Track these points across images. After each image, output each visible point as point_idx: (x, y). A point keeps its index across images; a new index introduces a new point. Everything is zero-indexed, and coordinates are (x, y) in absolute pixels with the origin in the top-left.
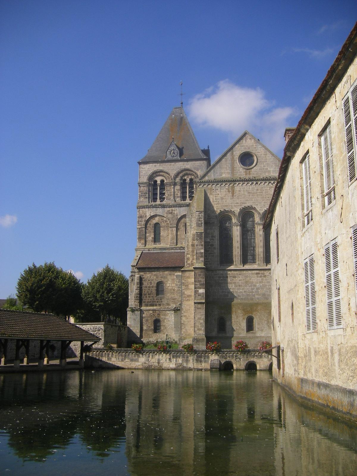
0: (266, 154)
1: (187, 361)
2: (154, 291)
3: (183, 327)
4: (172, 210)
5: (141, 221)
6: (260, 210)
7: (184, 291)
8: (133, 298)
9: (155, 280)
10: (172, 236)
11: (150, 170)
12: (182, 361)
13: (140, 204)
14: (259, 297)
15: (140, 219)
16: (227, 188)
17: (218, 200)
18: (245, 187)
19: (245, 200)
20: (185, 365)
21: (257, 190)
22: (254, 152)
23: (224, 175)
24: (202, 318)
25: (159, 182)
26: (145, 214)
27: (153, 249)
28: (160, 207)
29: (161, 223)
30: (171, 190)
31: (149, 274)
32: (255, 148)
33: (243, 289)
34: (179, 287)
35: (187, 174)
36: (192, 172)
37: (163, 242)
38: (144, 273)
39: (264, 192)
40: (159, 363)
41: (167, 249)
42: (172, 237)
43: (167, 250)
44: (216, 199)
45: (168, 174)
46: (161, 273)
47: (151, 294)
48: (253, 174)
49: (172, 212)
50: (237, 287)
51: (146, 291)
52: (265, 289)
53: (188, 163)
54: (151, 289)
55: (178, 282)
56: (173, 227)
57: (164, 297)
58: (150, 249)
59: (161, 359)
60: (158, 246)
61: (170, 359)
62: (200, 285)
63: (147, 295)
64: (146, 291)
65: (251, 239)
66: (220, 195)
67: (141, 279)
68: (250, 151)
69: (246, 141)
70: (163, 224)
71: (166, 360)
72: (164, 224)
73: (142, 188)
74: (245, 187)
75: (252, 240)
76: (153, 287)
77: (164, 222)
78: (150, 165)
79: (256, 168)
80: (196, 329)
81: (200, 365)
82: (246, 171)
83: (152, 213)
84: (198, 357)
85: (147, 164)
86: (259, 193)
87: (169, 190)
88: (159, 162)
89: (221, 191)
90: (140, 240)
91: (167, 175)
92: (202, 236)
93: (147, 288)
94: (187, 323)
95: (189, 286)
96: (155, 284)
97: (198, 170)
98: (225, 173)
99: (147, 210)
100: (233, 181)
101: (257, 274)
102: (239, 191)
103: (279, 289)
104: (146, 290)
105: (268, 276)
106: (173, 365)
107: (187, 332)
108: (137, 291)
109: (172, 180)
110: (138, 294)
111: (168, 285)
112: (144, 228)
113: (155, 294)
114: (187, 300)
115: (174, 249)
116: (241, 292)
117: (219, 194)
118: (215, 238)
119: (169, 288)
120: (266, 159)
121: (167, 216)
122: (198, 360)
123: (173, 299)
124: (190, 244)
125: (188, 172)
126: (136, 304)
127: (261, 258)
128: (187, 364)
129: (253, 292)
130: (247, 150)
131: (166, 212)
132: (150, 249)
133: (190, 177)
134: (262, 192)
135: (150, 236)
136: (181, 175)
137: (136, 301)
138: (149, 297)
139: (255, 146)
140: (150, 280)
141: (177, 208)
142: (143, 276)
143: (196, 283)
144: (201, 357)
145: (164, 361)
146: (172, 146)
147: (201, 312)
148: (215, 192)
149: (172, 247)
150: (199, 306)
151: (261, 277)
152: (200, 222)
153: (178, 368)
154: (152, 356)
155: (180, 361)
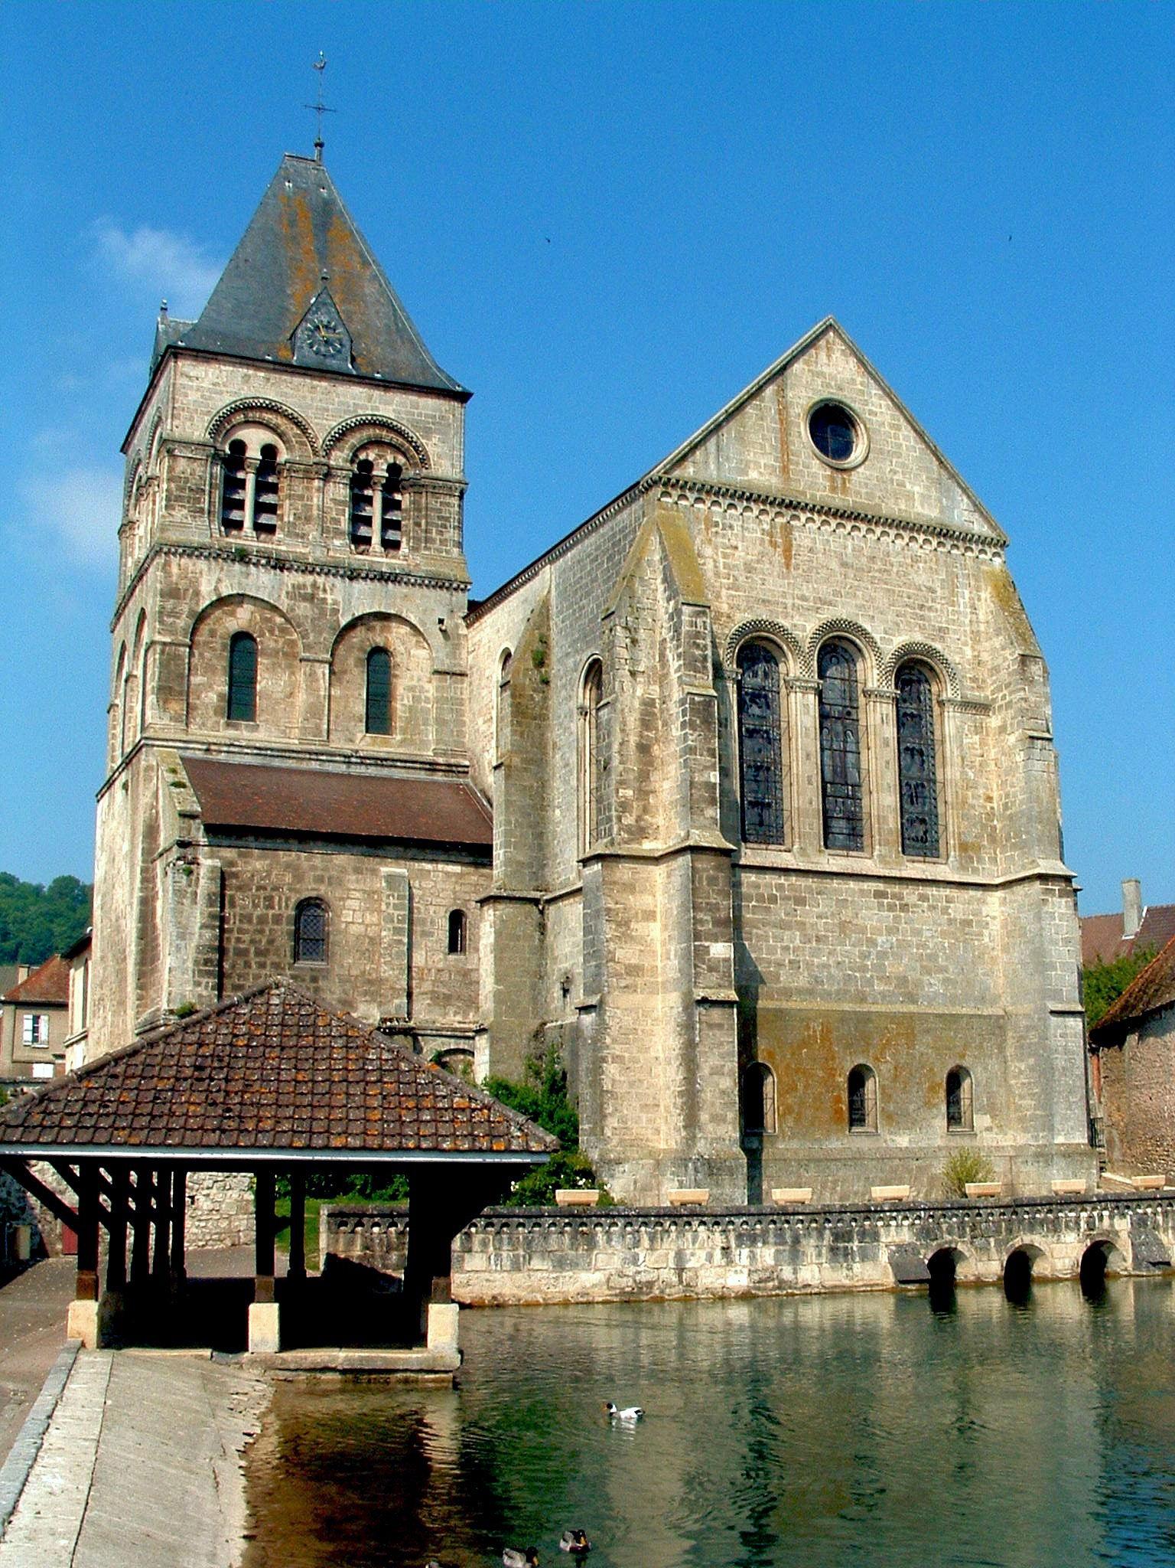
0: (898, 428)
1: (795, 1256)
2: (286, 944)
4: (314, 585)
5: (174, 614)
7: (612, 946)
8: (190, 964)
11: (221, 393)
12: (776, 1259)
13: (174, 536)
14: (886, 988)
15: (170, 604)
16: (766, 527)
18: (831, 539)
19: (830, 590)
20: (787, 1273)
21: (873, 559)
22: (856, 406)
23: (753, 475)
24: (726, 1070)
25: (254, 453)
26: (194, 584)
27: (225, 749)
28: (263, 561)
29: (262, 635)
30: (310, 499)
31: (260, 858)
34: (397, 931)
35: (378, 443)
36: (401, 440)
37: (266, 721)
38: (240, 855)
40: (680, 1270)
41: (284, 753)
43: (289, 758)
44: (726, 566)
45: (298, 424)
46: (318, 860)
47: (268, 950)
48: (858, 493)
50: (810, 941)
51: (246, 937)
52: (905, 960)
53: (390, 395)
54: (270, 930)
56: (318, 661)
57: (326, 974)
58: (213, 747)
59: (688, 1252)
60: (246, 734)
61: (726, 1250)
62: (717, 923)
63: (252, 955)
64: (246, 937)
66: (743, 554)
67: (223, 878)
68: (852, 405)
69: (829, 356)
70: (267, 642)
71: (710, 1257)
72: (276, 641)
73: (182, 462)
74: (831, 539)
75: (849, 755)
76: (277, 919)
77: (277, 633)
78: (222, 367)
79: (868, 473)
81: (845, 1272)
84: (837, 1236)
85: (207, 360)
86: (879, 571)
87: (301, 498)
88: (267, 365)
89: (743, 536)
91: (292, 431)
92: (711, 715)
93: (250, 921)
94: (625, 1088)
95: (633, 925)
96: (287, 906)
97: (428, 432)
99: (202, 564)
100: (790, 505)
101: (879, 894)
102: (811, 550)
104: (246, 932)
105: (915, 906)
106: (738, 1280)
108: (208, 934)
109: (315, 453)
110: (211, 948)
111: (347, 916)
112: (184, 645)
113: (288, 954)
115: (324, 758)
116: (826, 966)
121: (293, 610)
122: (839, 1253)
123: (370, 982)
124: (633, 739)
125: (384, 433)
126: (200, 996)
127: (890, 831)
128: (795, 1272)
129: (863, 969)
130: (838, 396)
131: (290, 589)
132: (213, 747)
135: (212, 688)
136: (354, 440)
137: (204, 981)
138: (262, 966)
140: (265, 889)
141: (338, 581)
142: (232, 864)
143: (700, 916)
144: (847, 1236)
145: (703, 1260)
146: (318, 309)
147: (721, 1044)
148: (724, 536)
149: (313, 747)
150: (716, 1014)
151: (891, 908)
152: (698, 652)
153: (759, 1289)
154: (652, 1239)
155: (767, 1255)
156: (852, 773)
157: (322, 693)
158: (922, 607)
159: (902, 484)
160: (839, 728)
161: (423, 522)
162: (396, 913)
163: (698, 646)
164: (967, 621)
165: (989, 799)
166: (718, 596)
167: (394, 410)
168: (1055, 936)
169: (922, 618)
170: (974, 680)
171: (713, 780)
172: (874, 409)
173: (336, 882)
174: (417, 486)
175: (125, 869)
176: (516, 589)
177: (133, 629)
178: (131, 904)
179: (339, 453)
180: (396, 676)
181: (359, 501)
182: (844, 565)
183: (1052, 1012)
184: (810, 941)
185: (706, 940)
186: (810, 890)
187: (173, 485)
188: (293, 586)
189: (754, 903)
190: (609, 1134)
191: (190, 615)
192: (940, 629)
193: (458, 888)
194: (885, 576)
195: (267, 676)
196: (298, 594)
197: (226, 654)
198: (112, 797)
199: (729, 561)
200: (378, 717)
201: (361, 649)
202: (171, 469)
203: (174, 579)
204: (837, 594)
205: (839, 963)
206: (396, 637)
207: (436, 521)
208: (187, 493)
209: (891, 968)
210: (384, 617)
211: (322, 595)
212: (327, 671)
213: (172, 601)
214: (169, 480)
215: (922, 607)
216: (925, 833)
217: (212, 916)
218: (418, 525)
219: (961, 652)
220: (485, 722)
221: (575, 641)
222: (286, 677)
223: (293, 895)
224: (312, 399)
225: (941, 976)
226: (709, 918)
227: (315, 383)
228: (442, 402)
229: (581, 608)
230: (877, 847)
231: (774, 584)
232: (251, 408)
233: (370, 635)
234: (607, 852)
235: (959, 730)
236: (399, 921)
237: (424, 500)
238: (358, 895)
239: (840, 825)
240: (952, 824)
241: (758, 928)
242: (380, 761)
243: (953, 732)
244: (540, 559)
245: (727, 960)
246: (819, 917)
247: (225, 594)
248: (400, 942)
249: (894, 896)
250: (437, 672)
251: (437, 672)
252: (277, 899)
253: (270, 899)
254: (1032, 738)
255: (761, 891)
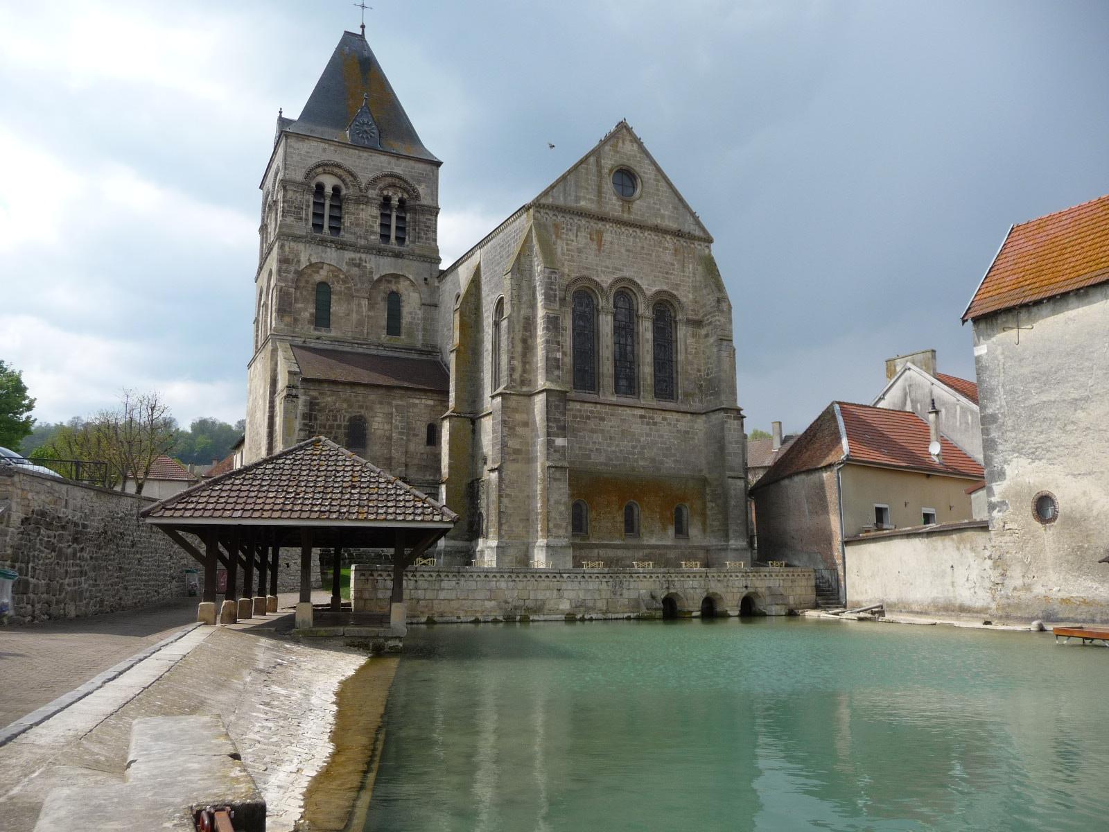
3: (504, 522)
5: (287, 271)
6: (646, 288)
9: (346, 412)
10: (359, 317)
11: (311, 157)
15: (284, 267)
17: (573, 254)
21: (643, 248)
22: (637, 169)
23: (583, 203)
24: (563, 501)
25: (328, 190)
26: (297, 255)
32: (640, 162)
33: (617, 446)
35: (393, 186)
39: (654, 254)
42: (359, 319)
45: (352, 175)
48: (636, 214)
49: (360, 264)
50: (606, 440)
52: (655, 450)
55: (400, 421)
62: (558, 428)
65: (626, 345)
70: (337, 287)
72: (341, 287)
76: (339, 427)
80: (551, 525)
82: (623, 205)
83: (315, 256)
86: (646, 254)
90: (282, 316)
91: (349, 179)
93: (325, 428)
95: (517, 429)
96: (344, 420)
97: (419, 182)
98: (585, 198)
99: (301, 247)
107: (513, 531)
109: (361, 190)
111: (375, 426)
114: (512, 460)
116: (614, 452)
117: (573, 241)
118: (566, 331)
119: (379, 432)
120: (658, 190)
121: (349, 271)
130: (627, 163)
131: (348, 261)
133: (400, 195)
134: (651, 255)
139: (638, 159)
142: (316, 398)
143: (550, 424)
146: (362, 115)
147: (560, 488)
151: (648, 424)
152: (552, 292)
156: (630, 357)
157: (364, 314)
158: (667, 273)
159: (659, 210)
160: (623, 333)
161: (417, 228)
162: (400, 424)
163: (552, 289)
164: (690, 281)
165: (699, 371)
166: (563, 265)
167: (402, 170)
168: (731, 440)
169: (667, 278)
170: (693, 310)
171: (558, 357)
172: (646, 171)
173: (368, 408)
174: (414, 210)
175: (261, 402)
176: (463, 262)
177: (266, 280)
178: (264, 420)
179: (373, 191)
180: (403, 306)
181: (385, 216)
182: (628, 250)
183: (729, 477)
184: (606, 440)
185: (553, 437)
186: (607, 413)
187: (285, 204)
188: (349, 259)
189: (578, 420)
190: (503, 533)
191: (296, 272)
192: (676, 284)
193: (432, 413)
194: (649, 257)
195: (335, 304)
196: (352, 263)
197: (314, 293)
198: (256, 367)
199: (570, 247)
200: (394, 326)
201: (385, 293)
202: (284, 196)
203: (287, 253)
204: (624, 265)
205: (621, 450)
206: (403, 287)
207: (423, 228)
208: (293, 209)
209: (647, 453)
210: (397, 276)
211: (364, 264)
212: (367, 303)
213: (286, 265)
214: (284, 202)
215: (667, 273)
216: (666, 387)
217: (305, 425)
218: (415, 230)
219: (686, 296)
220: (448, 330)
221: (492, 288)
222: (345, 306)
223: (347, 414)
224: (359, 163)
225: (672, 459)
226: (555, 425)
227: (361, 154)
228: (427, 165)
229: (495, 271)
230: (642, 393)
231: (590, 258)
232: (326, 165)
233: (389, 285)
234: (424, 349)
235: (685, 336)
236: (401, 428)
237: (417, 217)
238: (381, 415)
239: (623, 382)
240: (683, 384)
241: (580, 432)
242: (395, 349)
243: (682, 336)
244: (475, 247)
245: (563, 447)
246: (611, 427)
247: (313, 262)
248: (402, 439)
249: (650, 418)
250: (424, 304)
251: (424, 304)
252: (339, 417)
253: (336, 416)
254: (722, 339)
255: (582, 413)
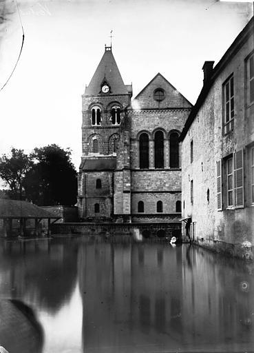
25: (96, 111)
103: (192, 181)
